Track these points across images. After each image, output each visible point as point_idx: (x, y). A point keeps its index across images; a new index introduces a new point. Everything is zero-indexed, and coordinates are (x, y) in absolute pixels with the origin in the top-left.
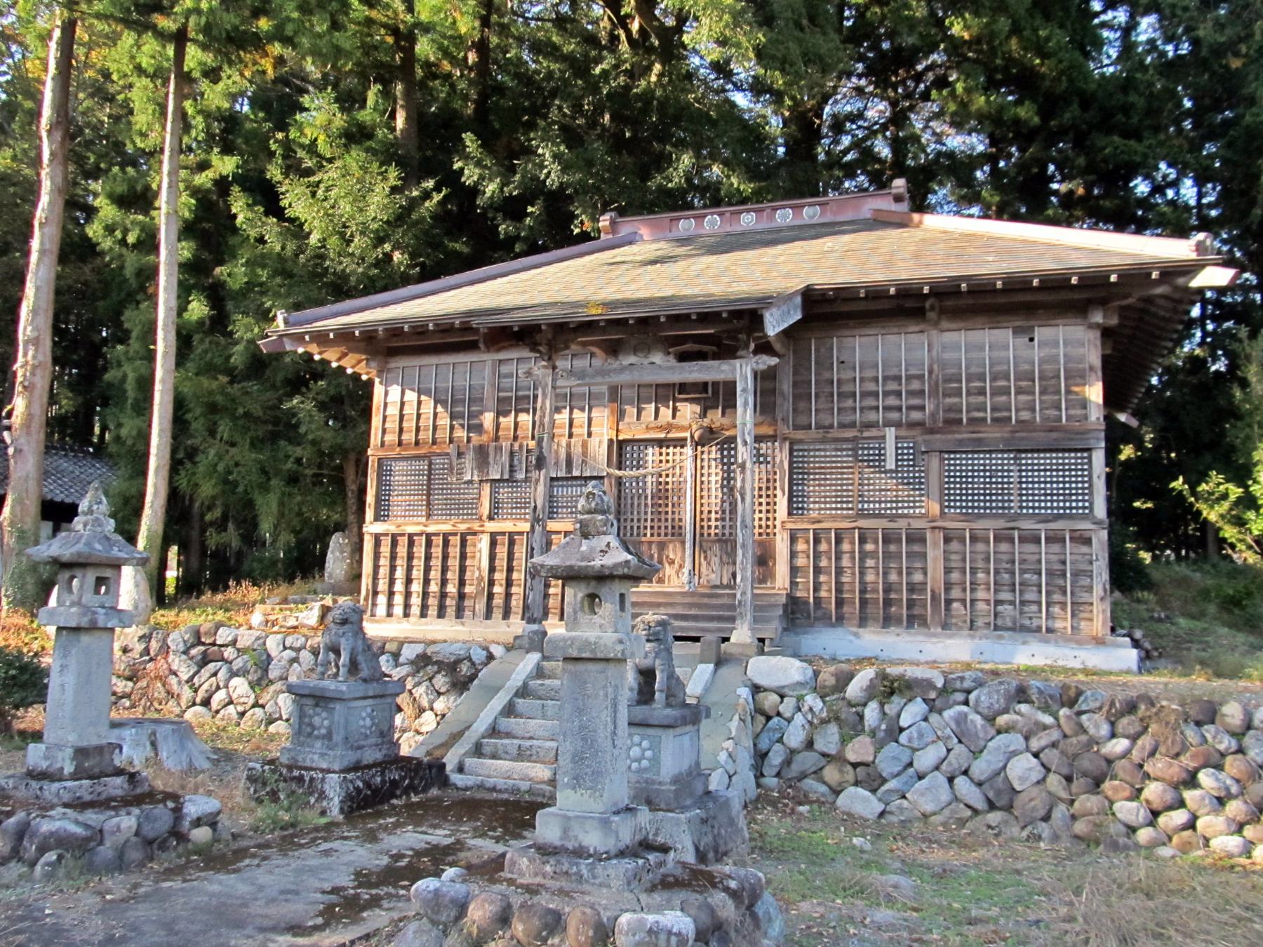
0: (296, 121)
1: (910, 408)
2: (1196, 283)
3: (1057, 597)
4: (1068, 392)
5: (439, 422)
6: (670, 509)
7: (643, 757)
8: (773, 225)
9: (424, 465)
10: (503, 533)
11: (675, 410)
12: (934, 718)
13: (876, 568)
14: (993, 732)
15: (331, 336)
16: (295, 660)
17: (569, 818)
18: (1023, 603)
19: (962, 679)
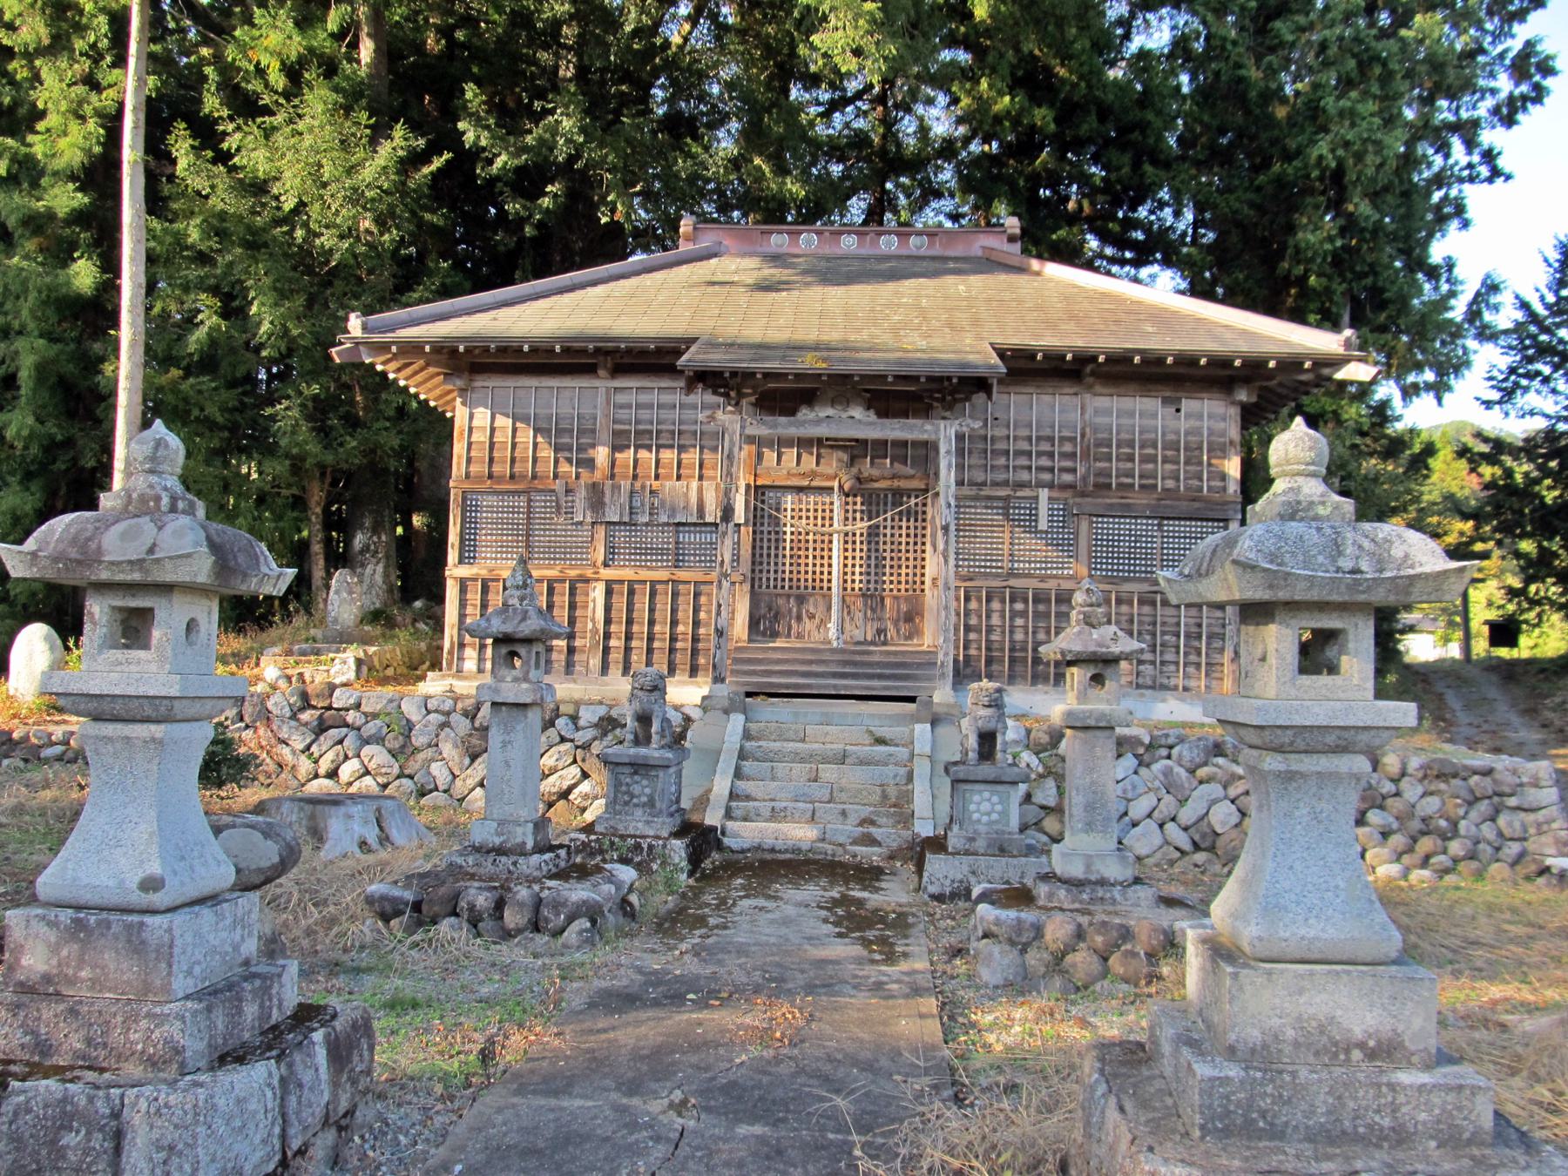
0: (234, 37)
1: (1062, 470)
2: (1340, 375)
3: (1193, 658)
4: (1209, 465)
5: (540, 454)
6: (810, 560)
7: (993, 811)
8: (877, 252)
9: (522, 502)
10: (622, 582)
11: (819, 457)
12: (1143, 771)
13: (1026, 627)
14: (1195, 783)
15: (427, 348)
16: (443, 725)
17: (1090, 856)
18: (1163, 663)
19: (1167, 736)
